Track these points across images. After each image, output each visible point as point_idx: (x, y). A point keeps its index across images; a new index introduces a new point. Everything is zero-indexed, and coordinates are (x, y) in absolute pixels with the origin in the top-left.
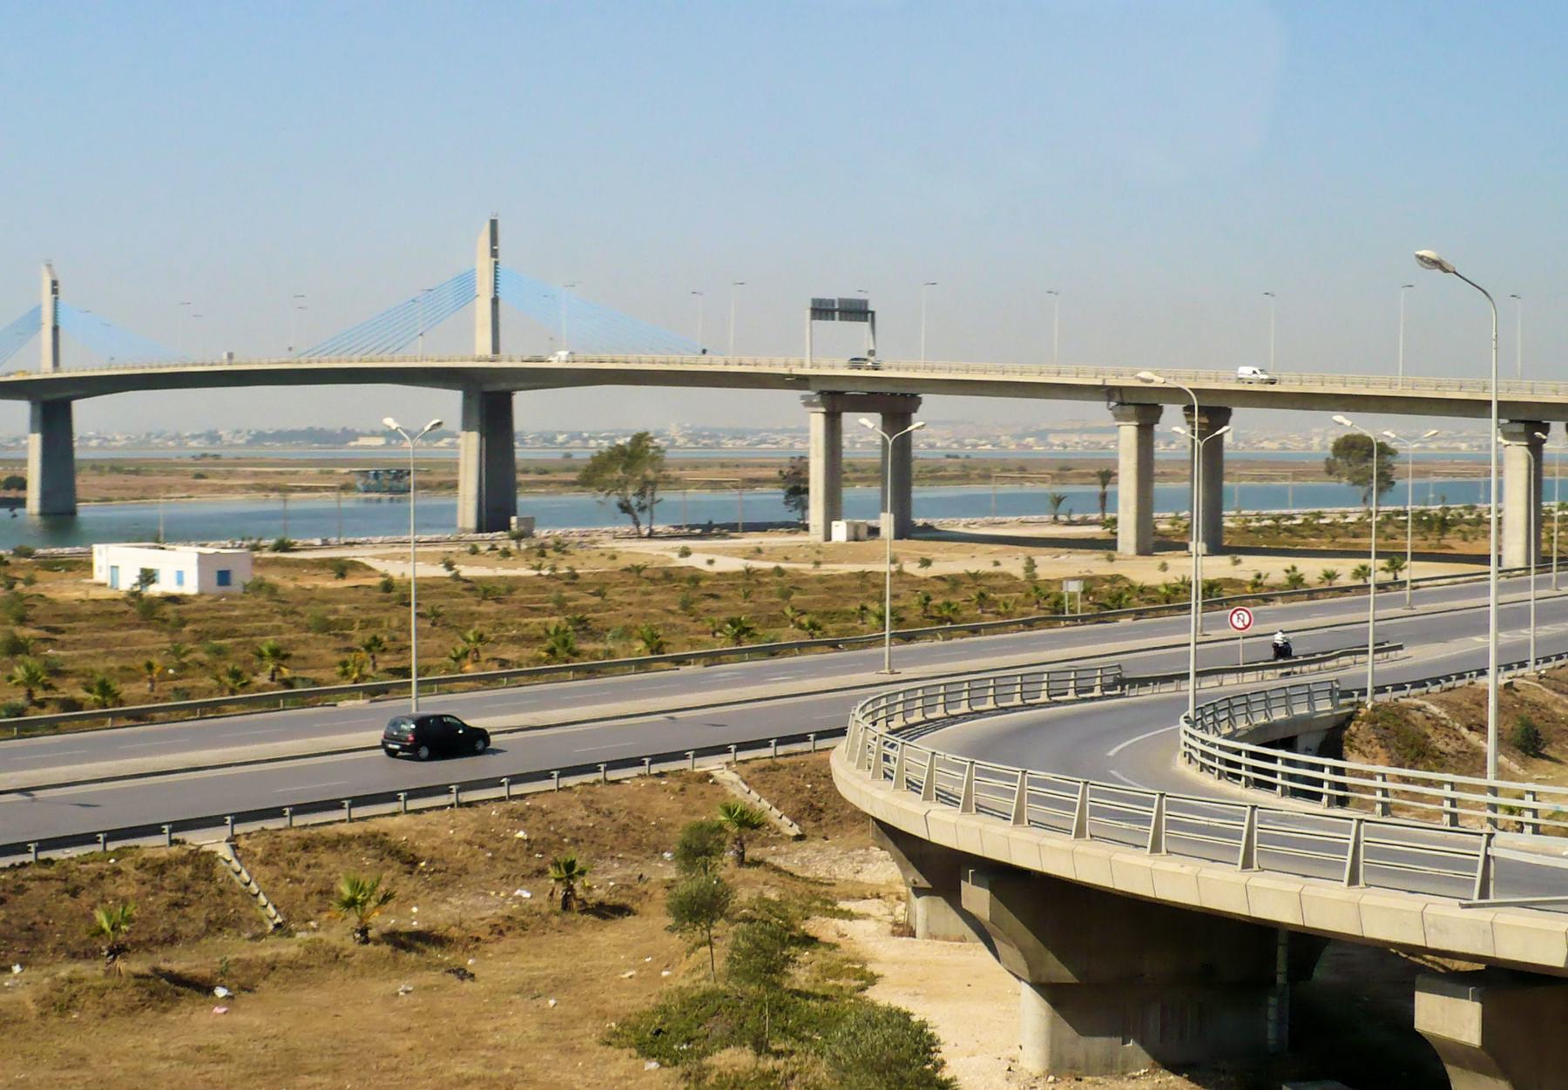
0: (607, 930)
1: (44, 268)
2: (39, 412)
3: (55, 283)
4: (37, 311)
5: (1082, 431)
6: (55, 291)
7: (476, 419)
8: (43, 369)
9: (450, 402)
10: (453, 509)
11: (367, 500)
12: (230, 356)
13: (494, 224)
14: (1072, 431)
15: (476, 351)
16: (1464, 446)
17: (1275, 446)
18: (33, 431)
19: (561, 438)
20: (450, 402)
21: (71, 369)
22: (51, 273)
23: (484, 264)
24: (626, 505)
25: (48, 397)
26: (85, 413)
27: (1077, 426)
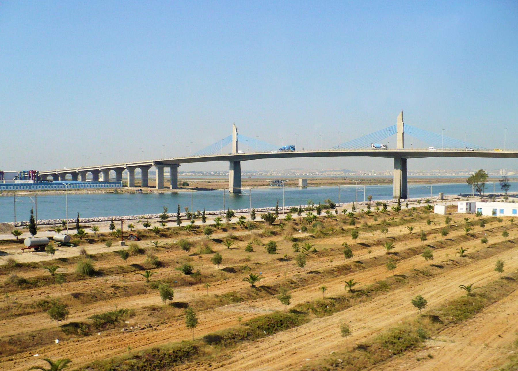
0: (318, 298)
1: (233, 125)
2: (233, 165)
3: (237, 129)
4: (231, 137)
5: (334, 171)
6: (237, 131)
7: (233, 168)
8: (234, 153)
9: (227, 164)
10: (391, 189)
11: (274, 188)
12: (303, 149)
13: (402, 112)
14: (331, 171)
15: (398, 147)
16: (422, 174)
17: (388, 174)
18: (230, 170)
19: (212, 173)
20: (392, 160)
21: (240, 152)
22: (235, 126)
23: (399, 124)
24: (506, 188)
25: (235, 160)
26: (244, 165)
27: (332, 170)
